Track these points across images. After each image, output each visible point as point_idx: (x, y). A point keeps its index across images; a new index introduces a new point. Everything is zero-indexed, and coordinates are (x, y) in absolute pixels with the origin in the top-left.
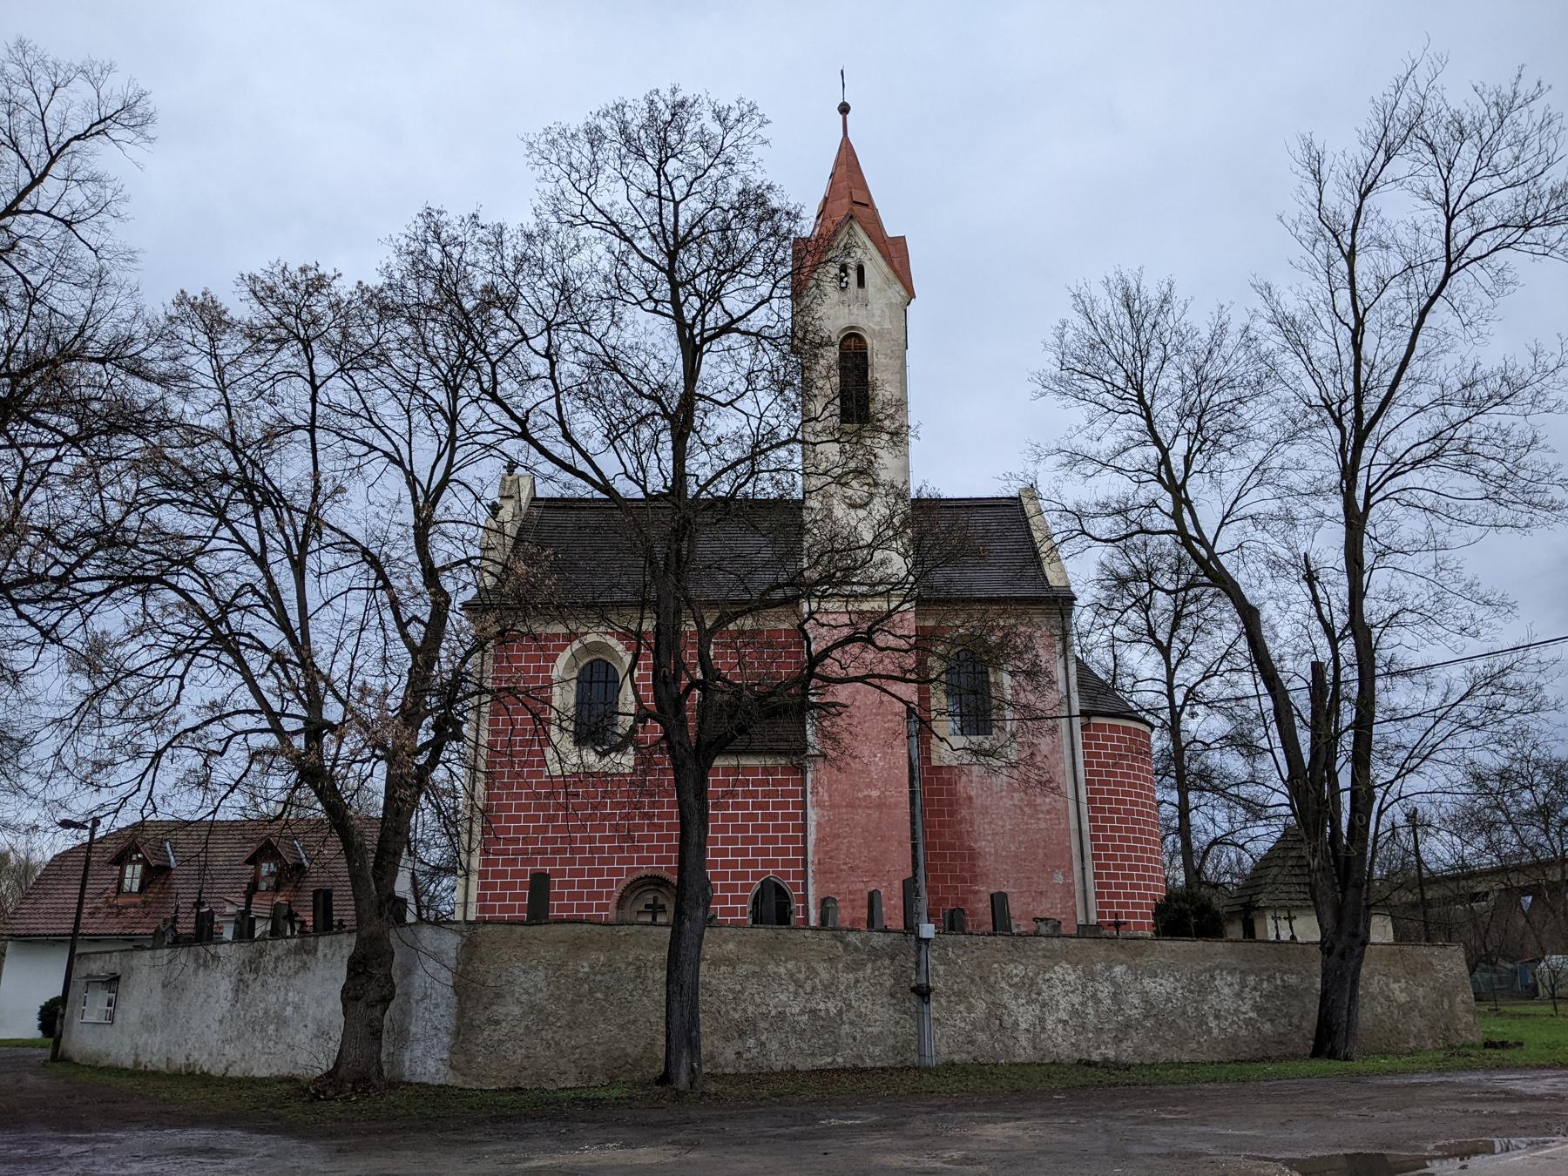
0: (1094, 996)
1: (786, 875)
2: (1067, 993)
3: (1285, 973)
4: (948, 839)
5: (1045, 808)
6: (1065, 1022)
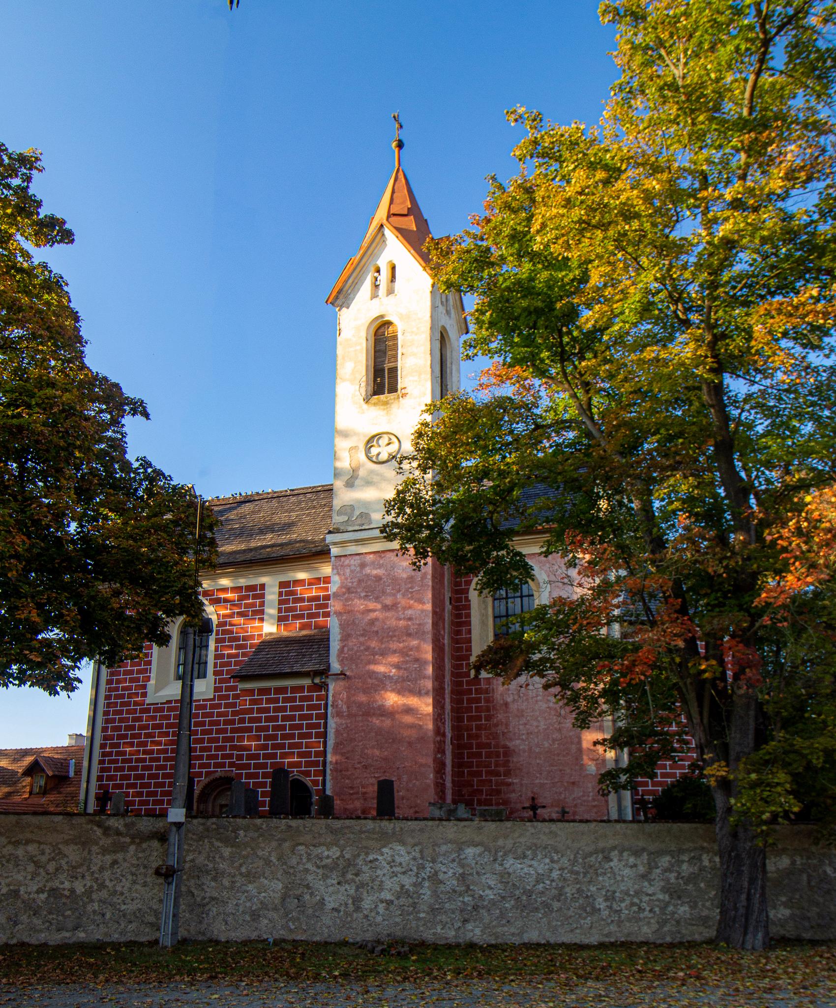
1: (308, 774)
4: (484, 740)
6: (389, 903)
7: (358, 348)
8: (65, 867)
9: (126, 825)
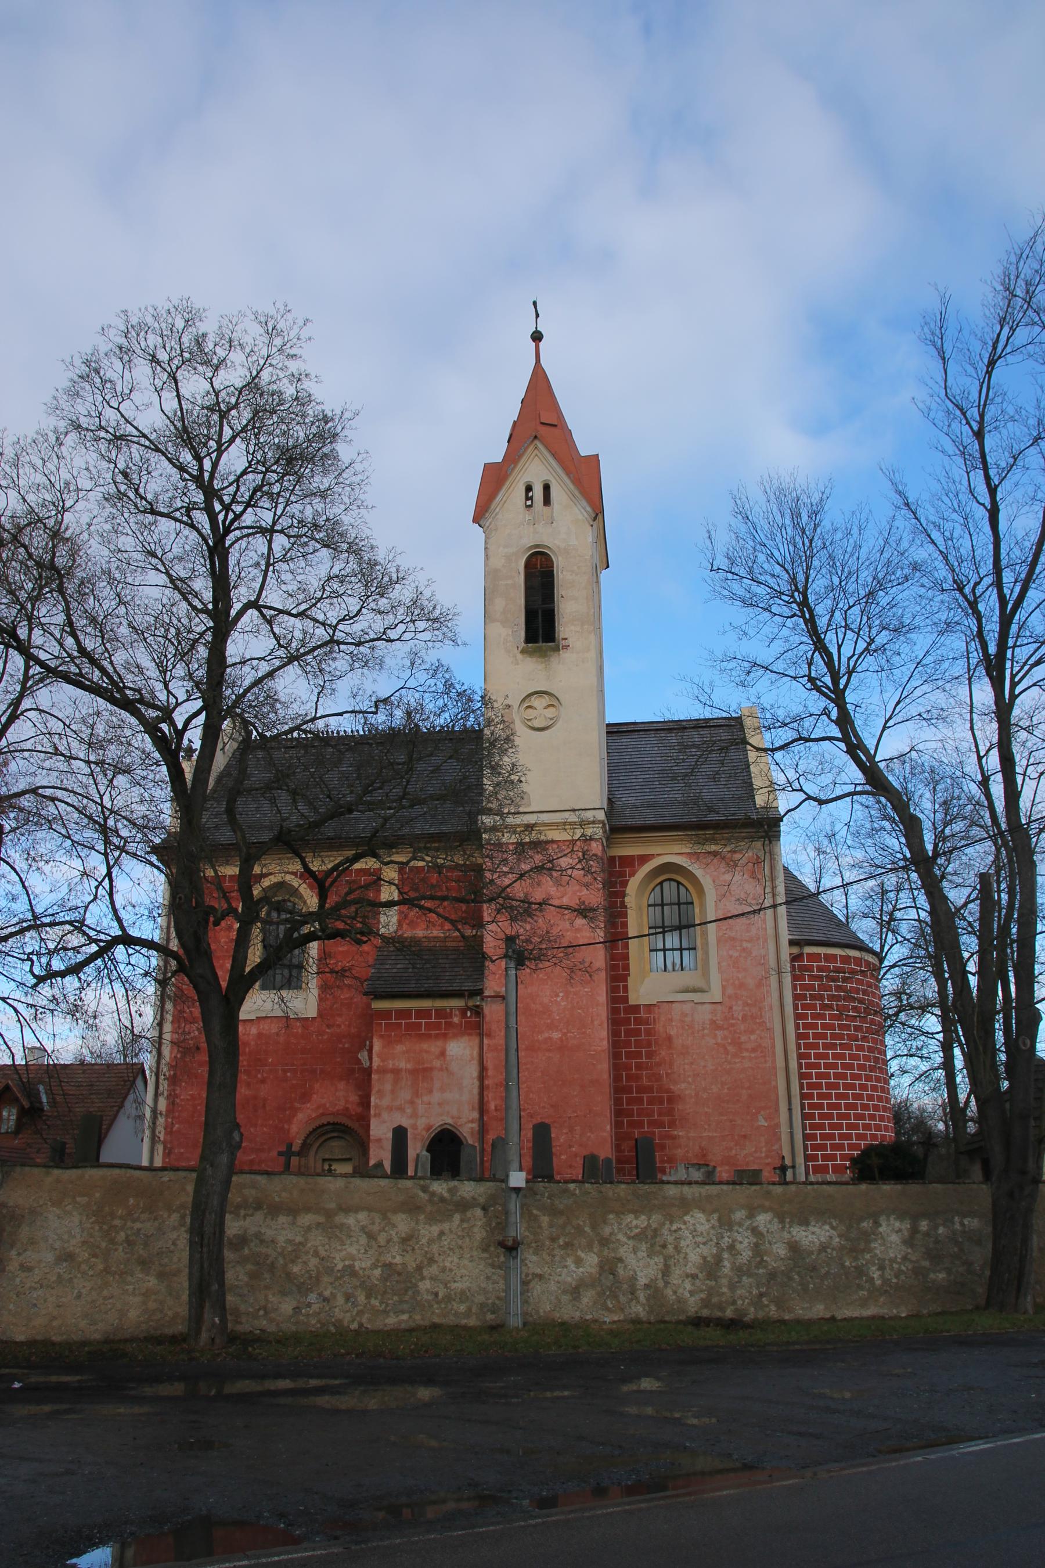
0: (731, 1247)
2: (697, 1245)
3: (965, 1216)
4: (645, 1082)
5: (749, 1046)
8: (396, 1239)
9: (450, 1190)
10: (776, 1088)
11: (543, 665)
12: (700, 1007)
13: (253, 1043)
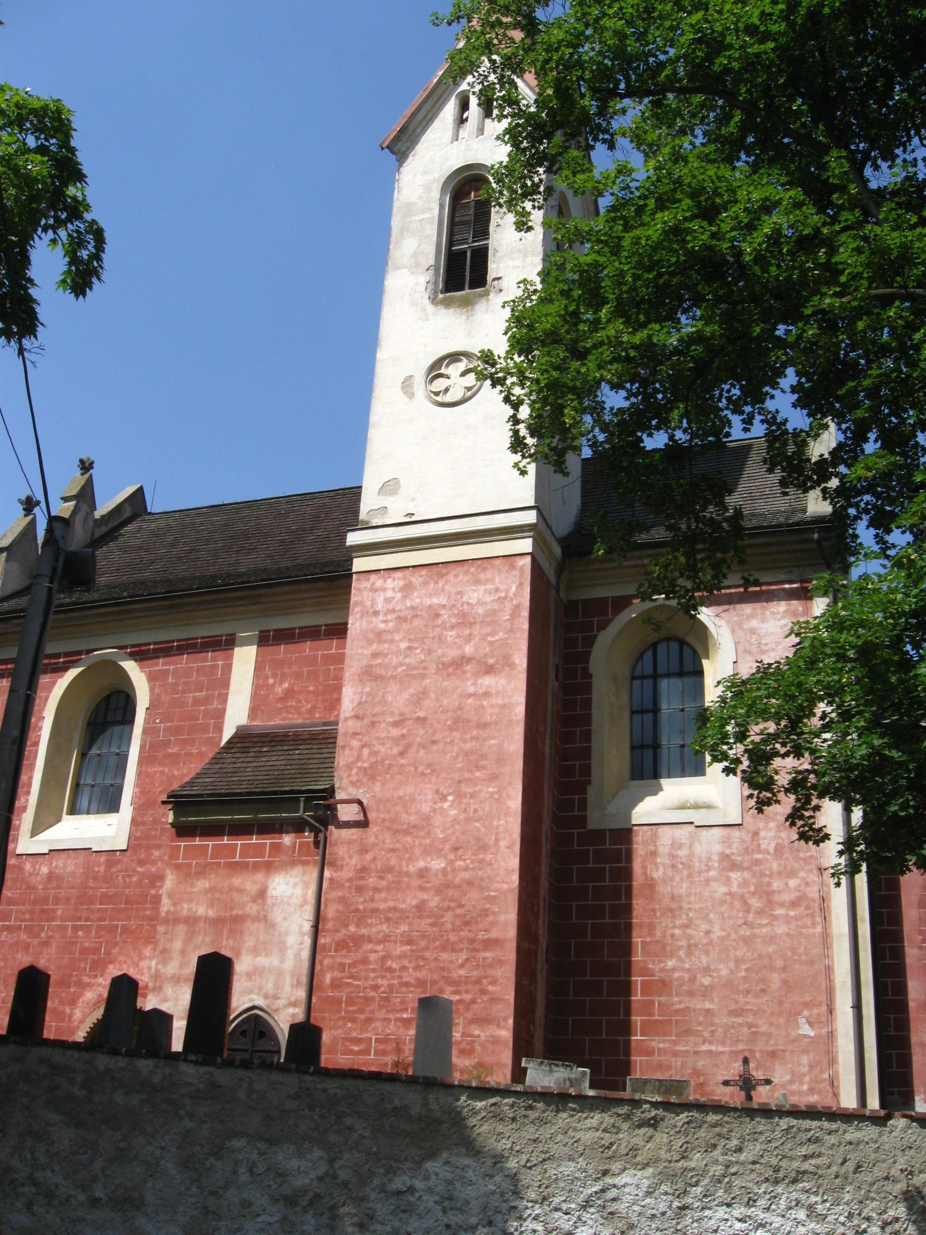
5: (786, 897)
7: (426, 216)
10: (829, 970)
11: (464, 317)
12: (704, 833)
13: (40, 887)
